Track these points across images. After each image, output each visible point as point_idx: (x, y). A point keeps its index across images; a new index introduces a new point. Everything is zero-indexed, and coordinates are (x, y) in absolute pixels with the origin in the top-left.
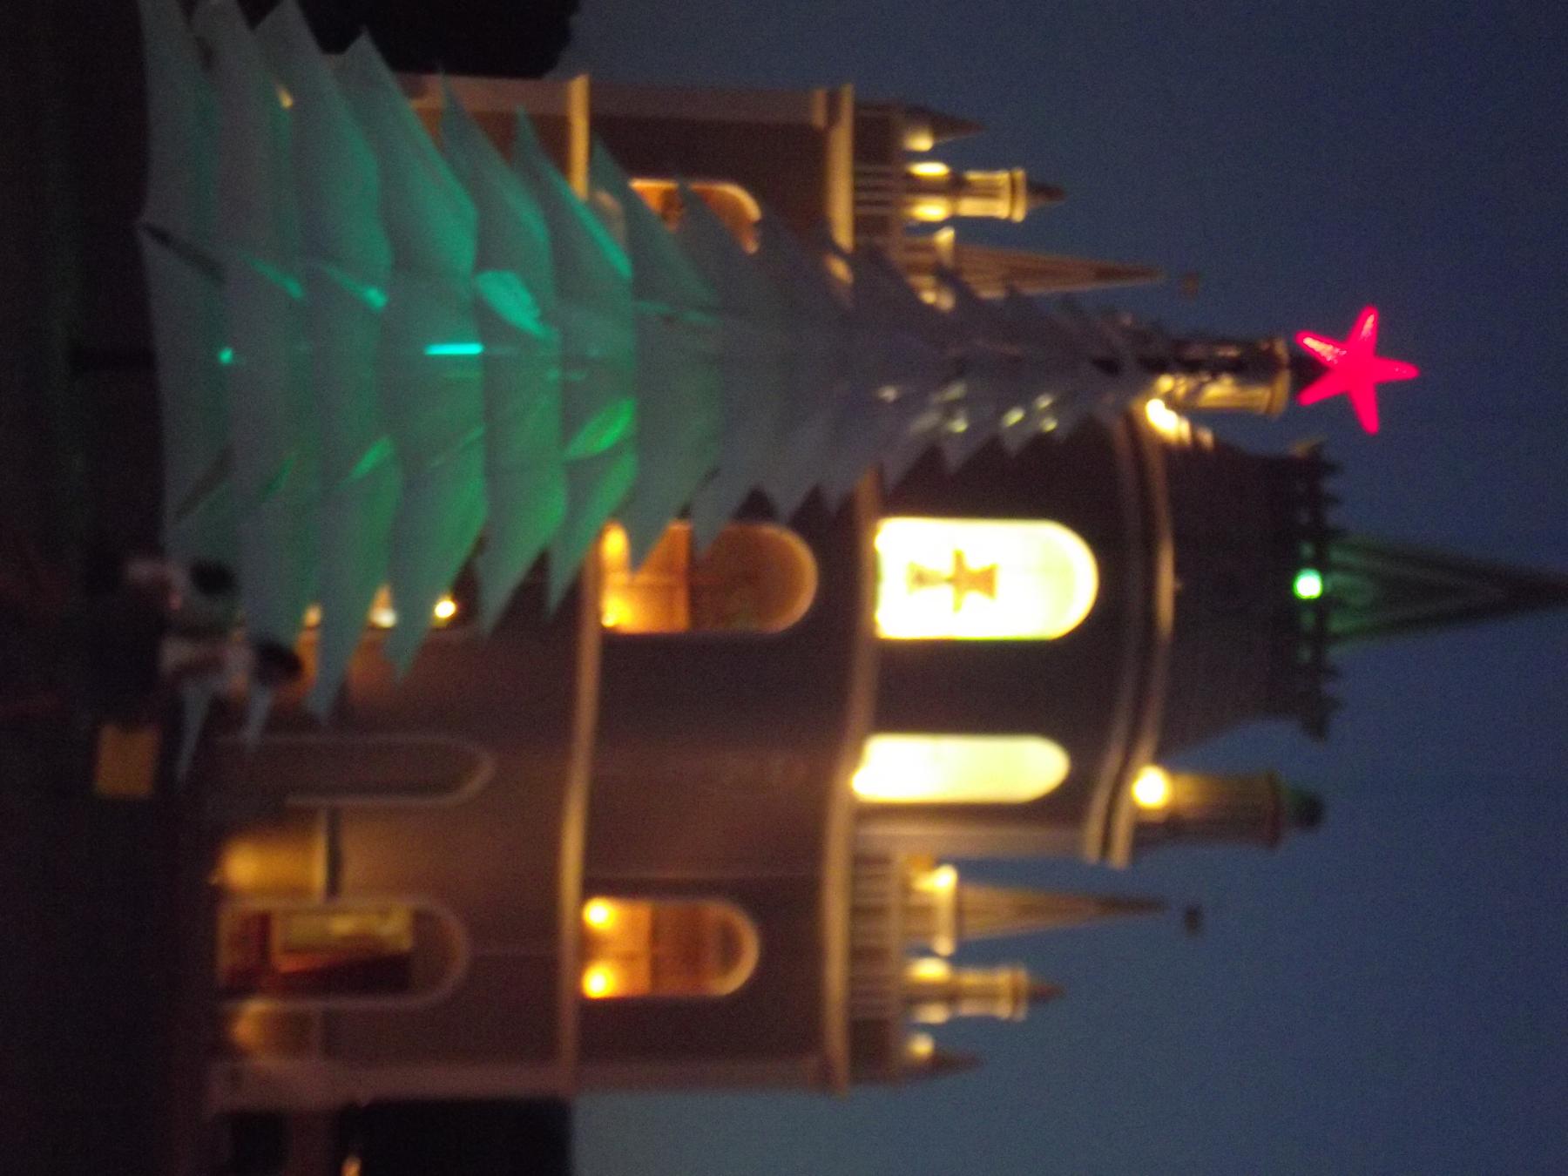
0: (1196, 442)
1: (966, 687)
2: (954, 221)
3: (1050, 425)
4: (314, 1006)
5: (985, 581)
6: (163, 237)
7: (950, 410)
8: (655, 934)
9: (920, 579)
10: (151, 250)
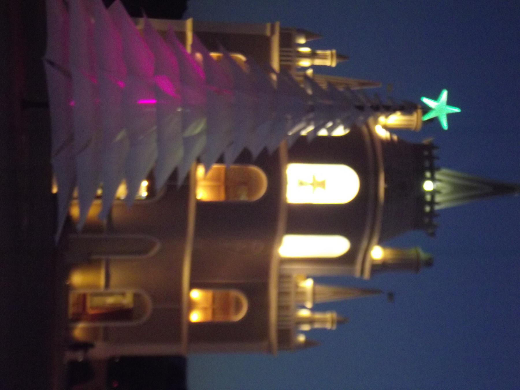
0: (392, 139)
1: (316, 219)
2: (313, 67)
4: (101, 325)
5: (322, 184)
6: (52, 63)
9: (301, 184)
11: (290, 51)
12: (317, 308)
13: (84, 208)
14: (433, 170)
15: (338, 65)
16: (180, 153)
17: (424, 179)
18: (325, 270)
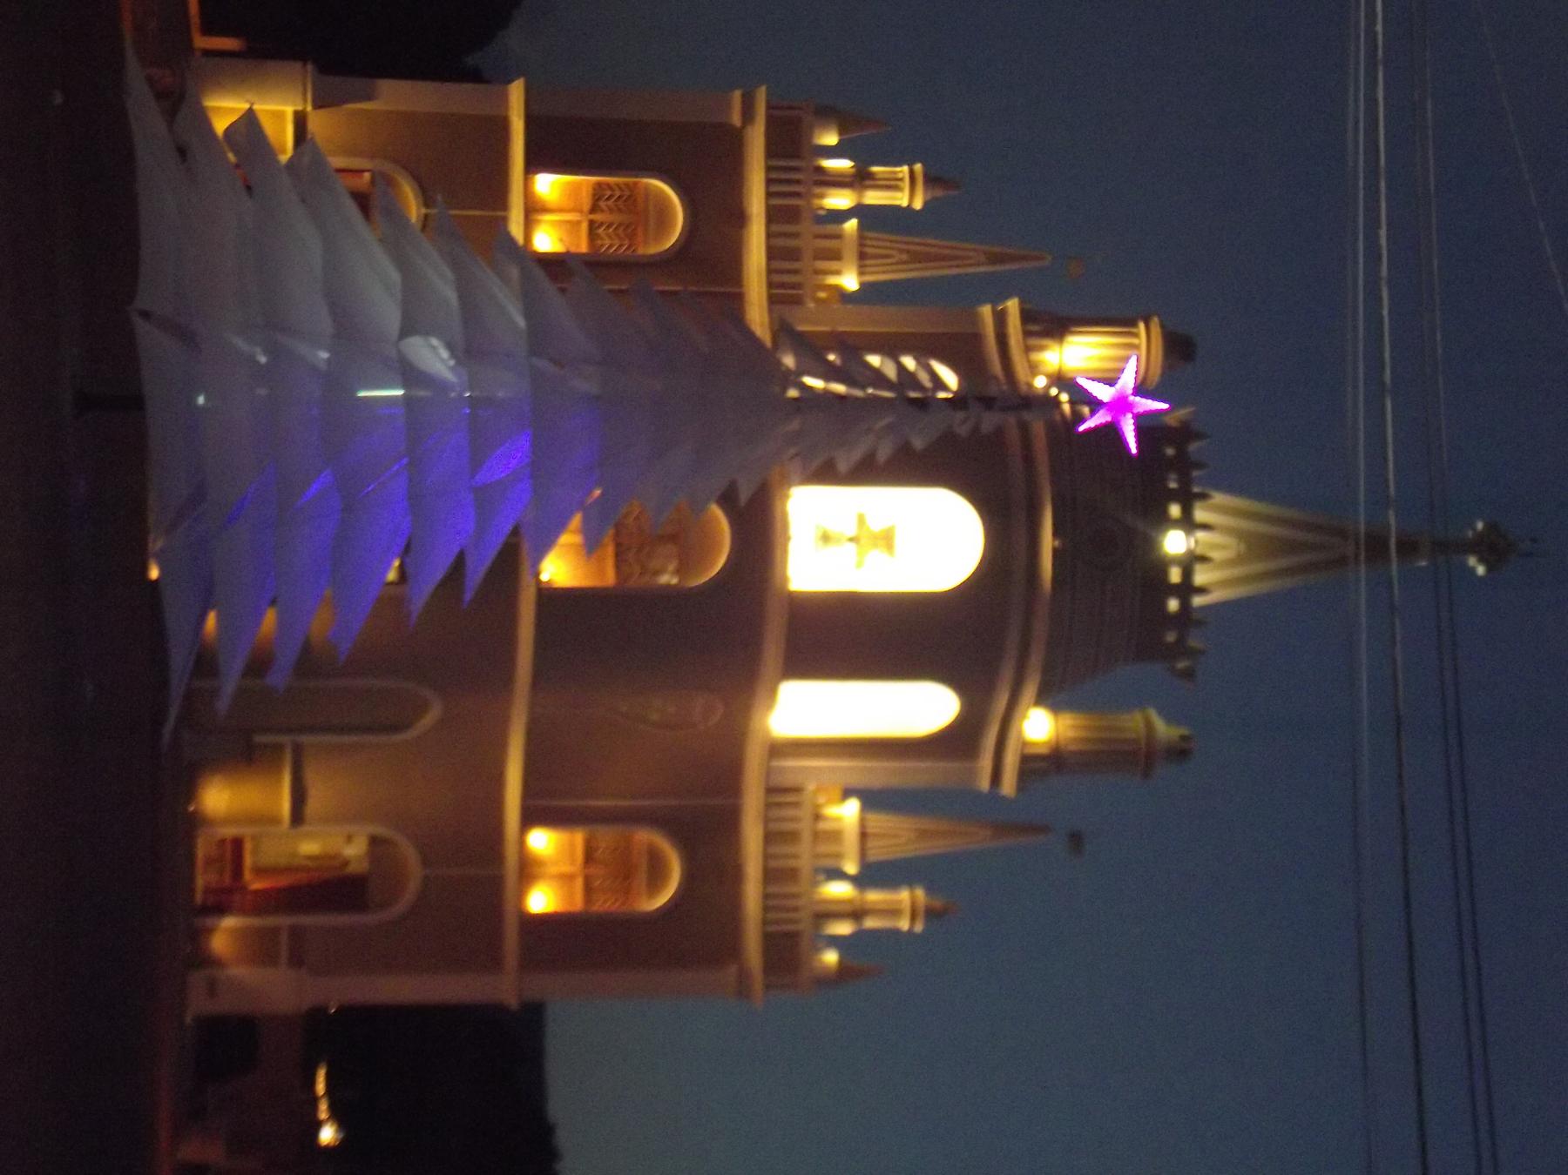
2: (859, 211)
4: (284, 921)
5: (886, 540)
6: (146, 315)
8: (589, 857)
9: (826, 538)
10: (142, 327)
12: (869, 876)
14: (1187, 500)
17: (1165, 522)
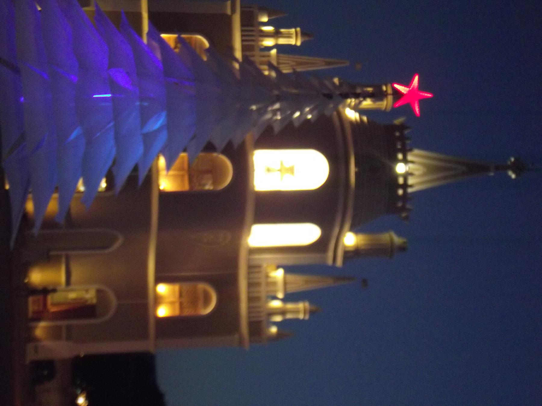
0: (361, 120)
2: (277, 46)
3: (309, 117)
4: (64, 323)
5: (291, 170)
7: (275, 112)
8: (181, 295)
9: (269, 170)
11: (253, 36)
12: (287, 298)
13: (40, 204)
14: (405, 152)
15: (302, 43)
16: (141, 150)
17: (397, 161)
18: (296, 260)
